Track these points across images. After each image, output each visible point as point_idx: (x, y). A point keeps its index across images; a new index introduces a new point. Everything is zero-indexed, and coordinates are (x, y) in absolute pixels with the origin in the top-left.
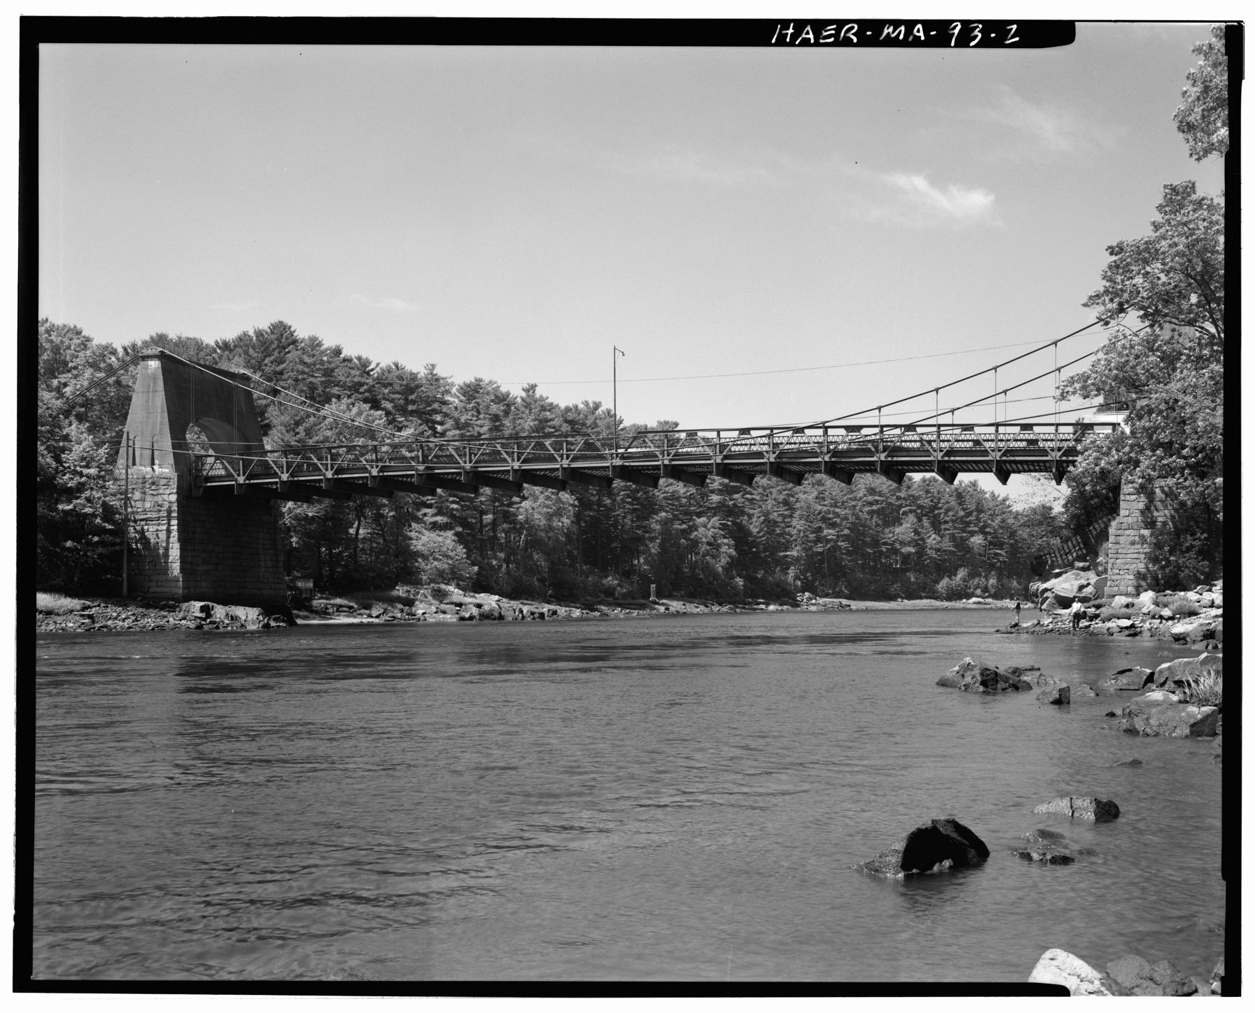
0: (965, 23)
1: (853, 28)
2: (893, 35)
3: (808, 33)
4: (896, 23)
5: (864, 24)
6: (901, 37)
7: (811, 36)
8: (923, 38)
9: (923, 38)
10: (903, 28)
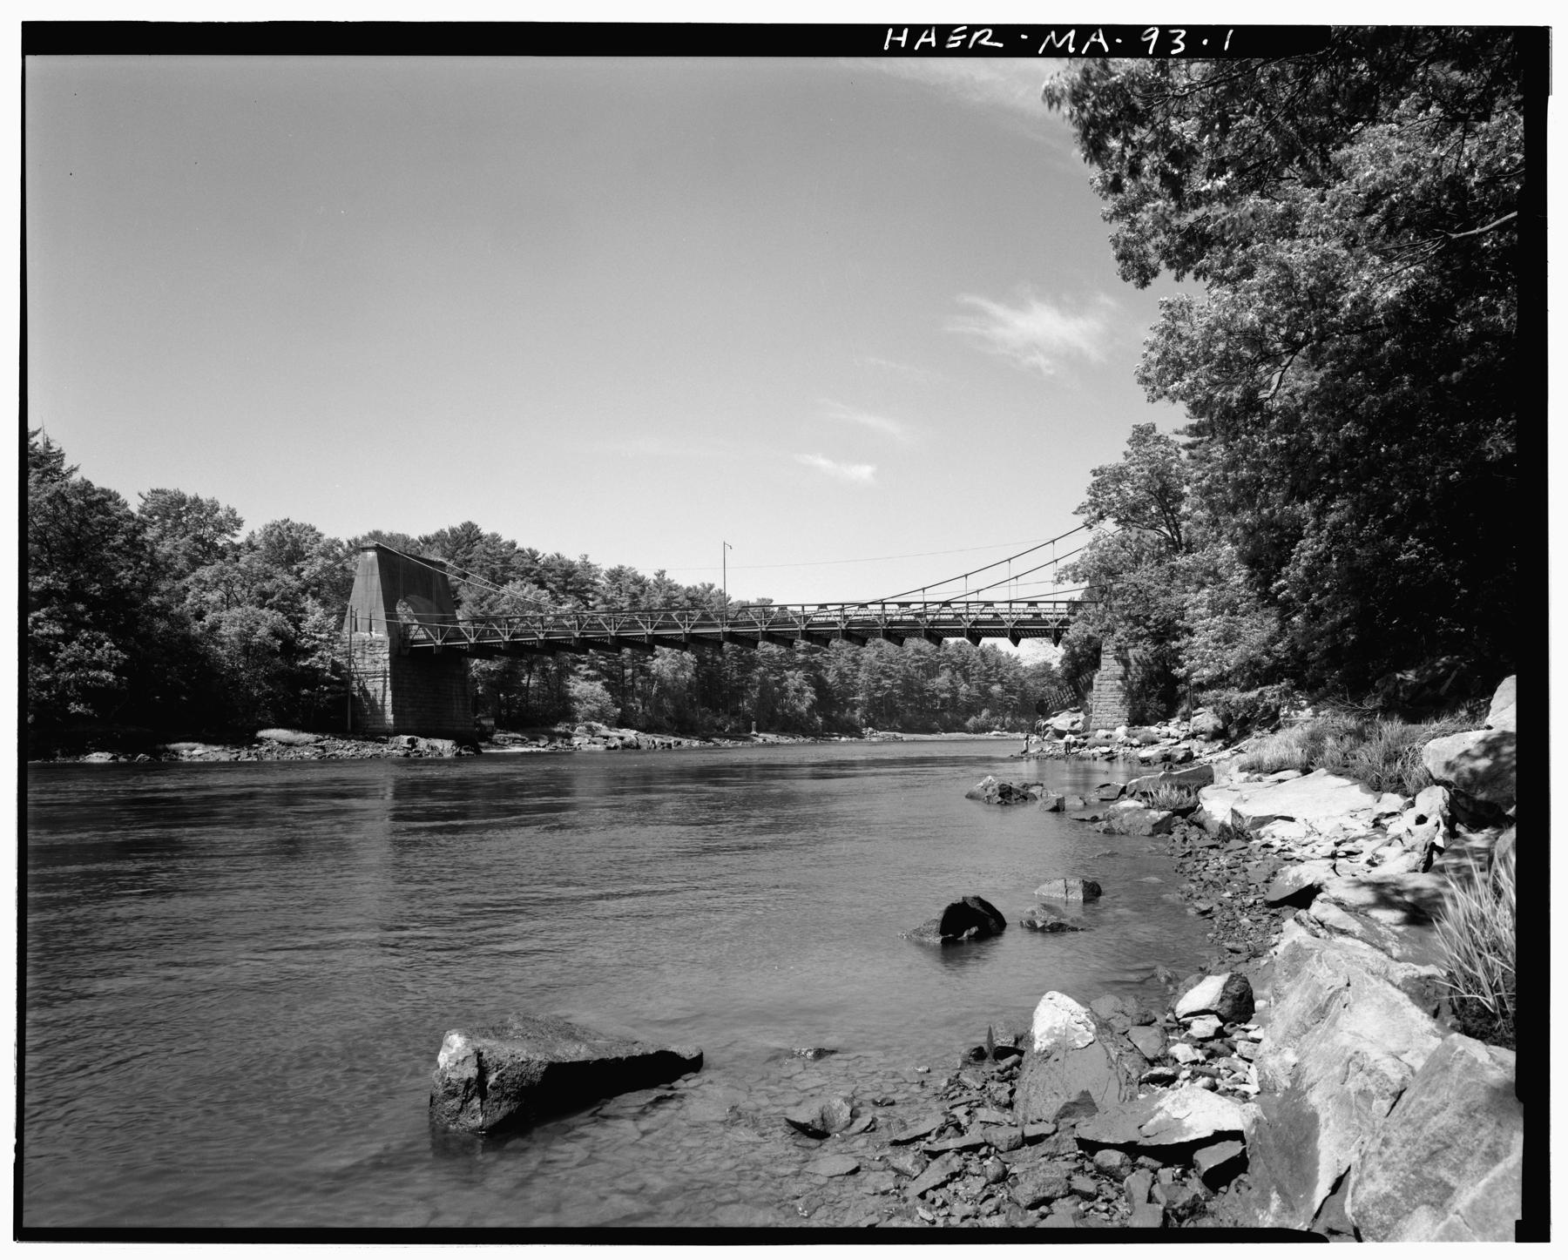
0: (1164, 29)
1: (987, 33)
2: (1059, 45)
3: (928, 36)
7: (932, 40)
10: (1053, 34)
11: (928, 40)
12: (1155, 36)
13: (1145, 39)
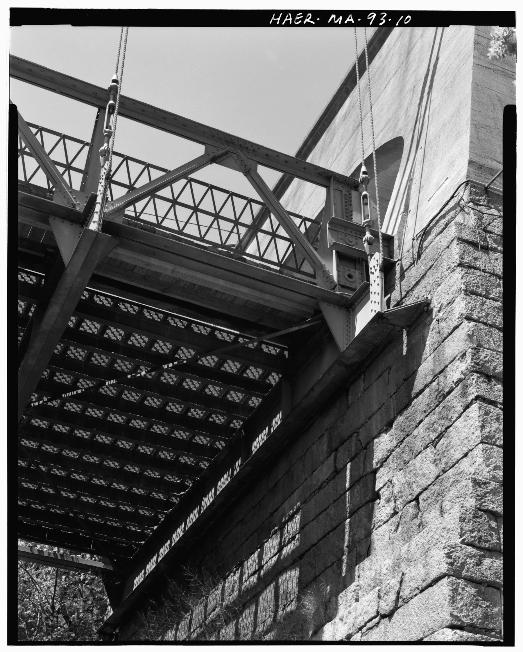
4: (338, 13)
5: (316, 13)
6: (340, 23)
8: (353, 22)
9: (353, 22)
13: (369, 18)
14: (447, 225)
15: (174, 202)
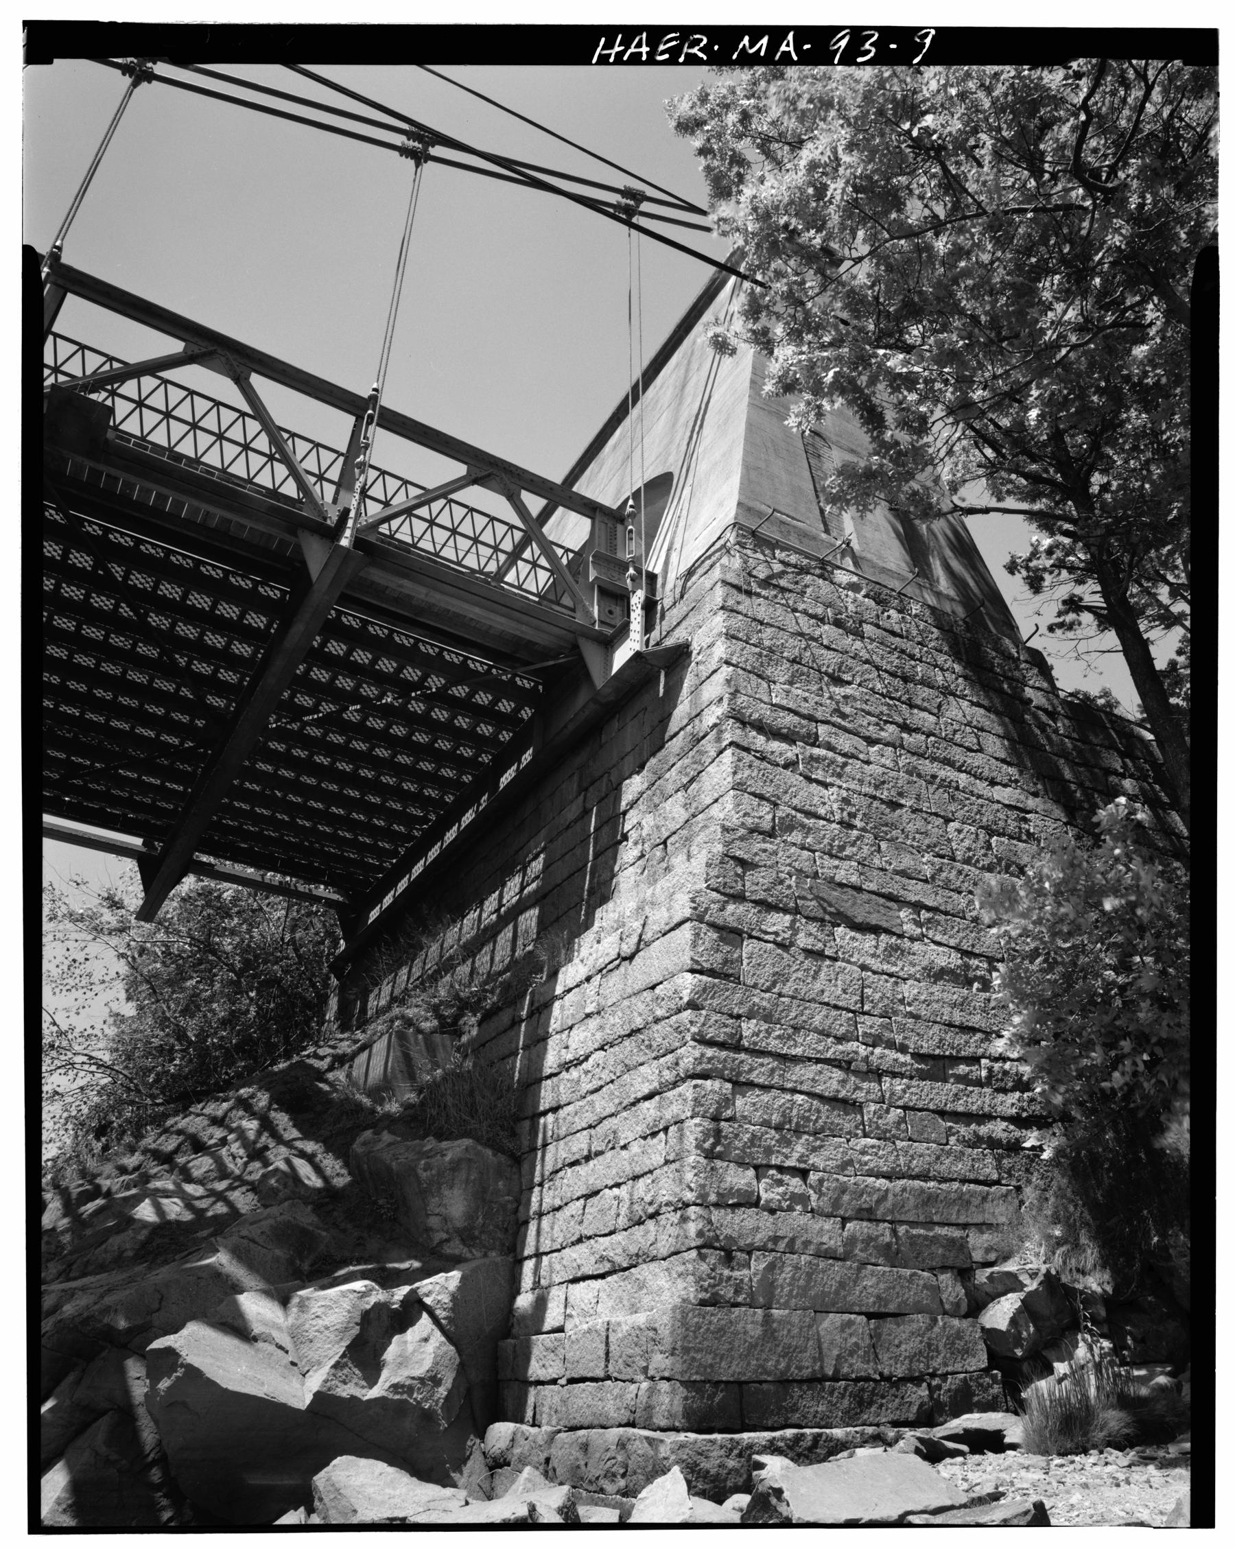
3: (639, 45)
11: (787, 49)
12: (843, 43)
14: (712, 566)
15: (432, 523)
